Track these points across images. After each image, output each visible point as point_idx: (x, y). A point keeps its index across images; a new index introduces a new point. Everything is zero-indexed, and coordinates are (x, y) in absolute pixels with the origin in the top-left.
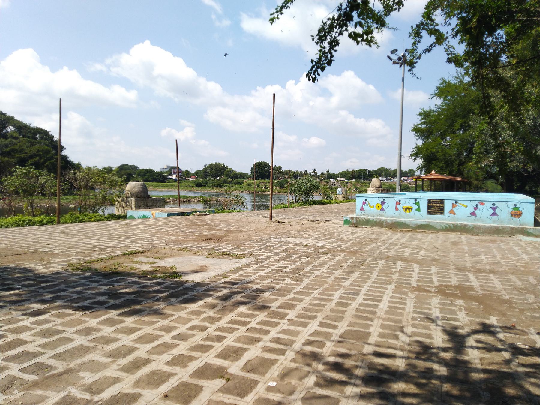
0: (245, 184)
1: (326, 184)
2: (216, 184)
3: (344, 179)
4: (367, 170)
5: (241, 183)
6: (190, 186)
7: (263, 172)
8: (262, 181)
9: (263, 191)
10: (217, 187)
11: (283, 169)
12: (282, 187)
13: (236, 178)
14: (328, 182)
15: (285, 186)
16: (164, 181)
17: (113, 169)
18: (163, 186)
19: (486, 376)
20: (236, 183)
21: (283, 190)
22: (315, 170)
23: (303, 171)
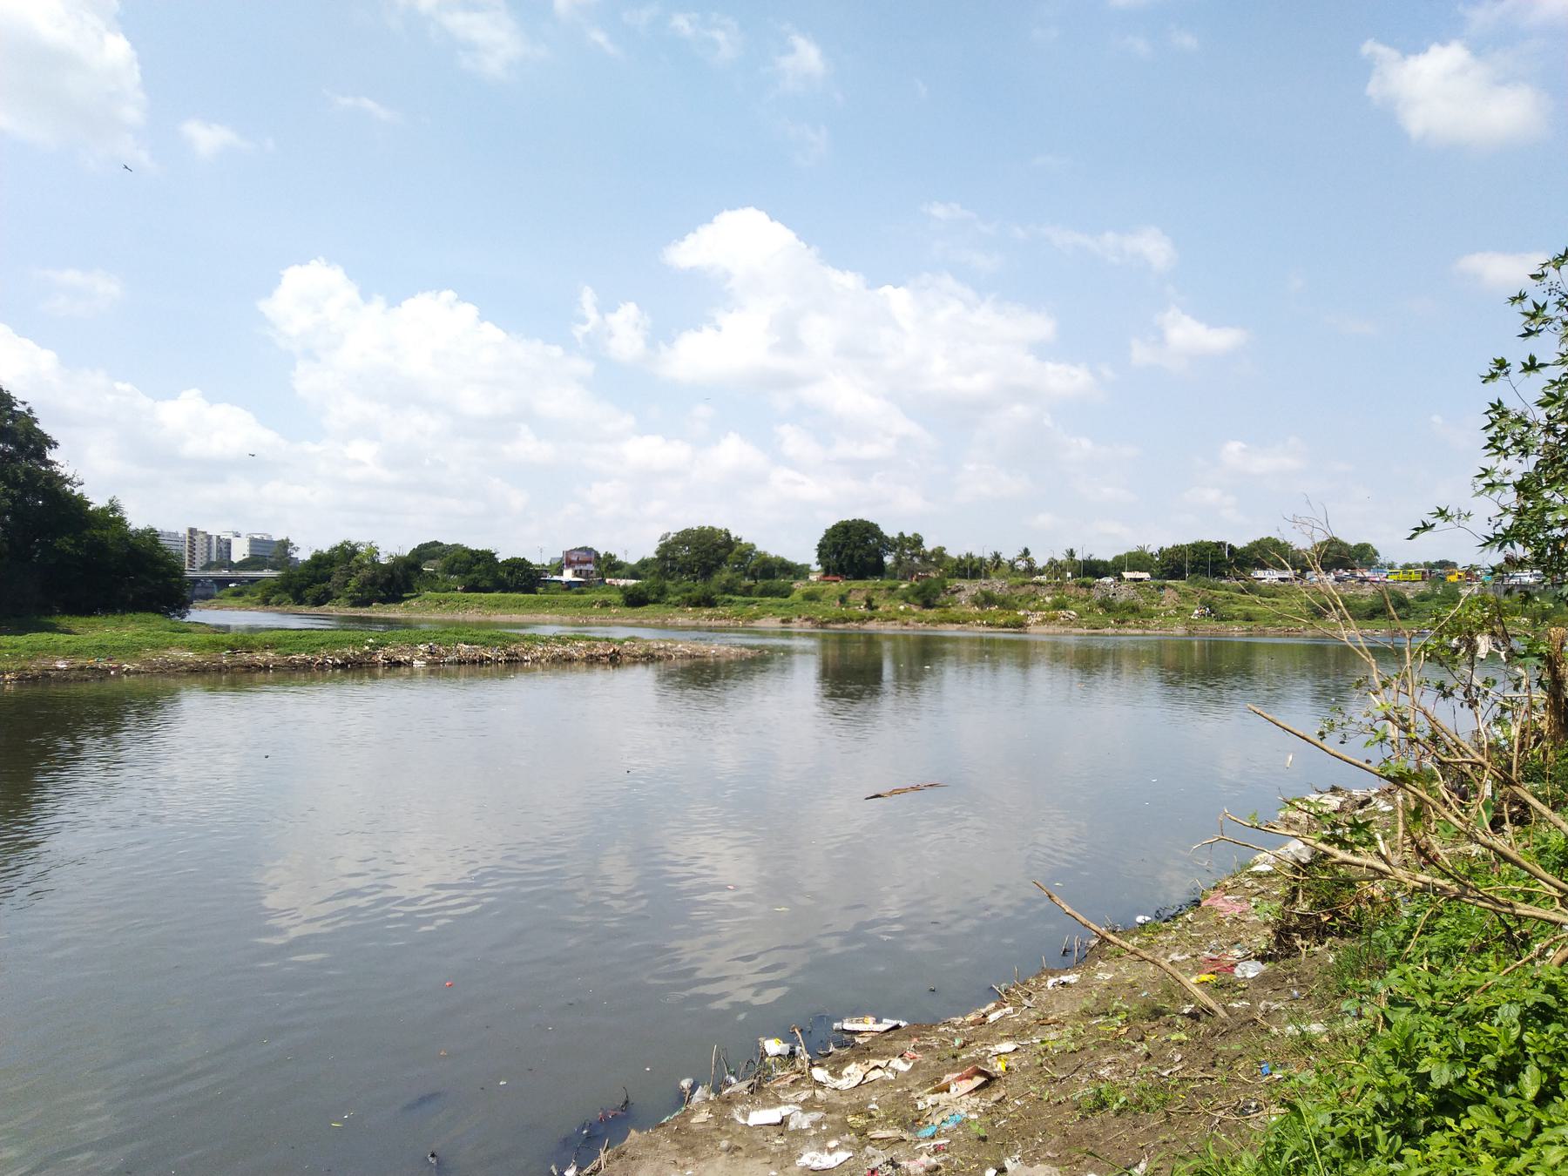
0: (796, 596)
1: (1083, 592)
2: (695, 594)
3: (1146, 575)
4: (1223, 544)
5: (785, 593)
6: (605, 604)
7: (858, 553)
8: (856, 584)
9: (862, 619)
10: (697, 604)
11: (929, 546)
12: (927, 605)
13: (769, 577)
14: (1090, 587)
15: (939, 602)
16: (529, 589)
17: (360, 549)
18: (518, 605)
19: (1268, 765)
20: (765, 593)
21: (931, 613)
22: (1026, 552)
23: (988, 556)
